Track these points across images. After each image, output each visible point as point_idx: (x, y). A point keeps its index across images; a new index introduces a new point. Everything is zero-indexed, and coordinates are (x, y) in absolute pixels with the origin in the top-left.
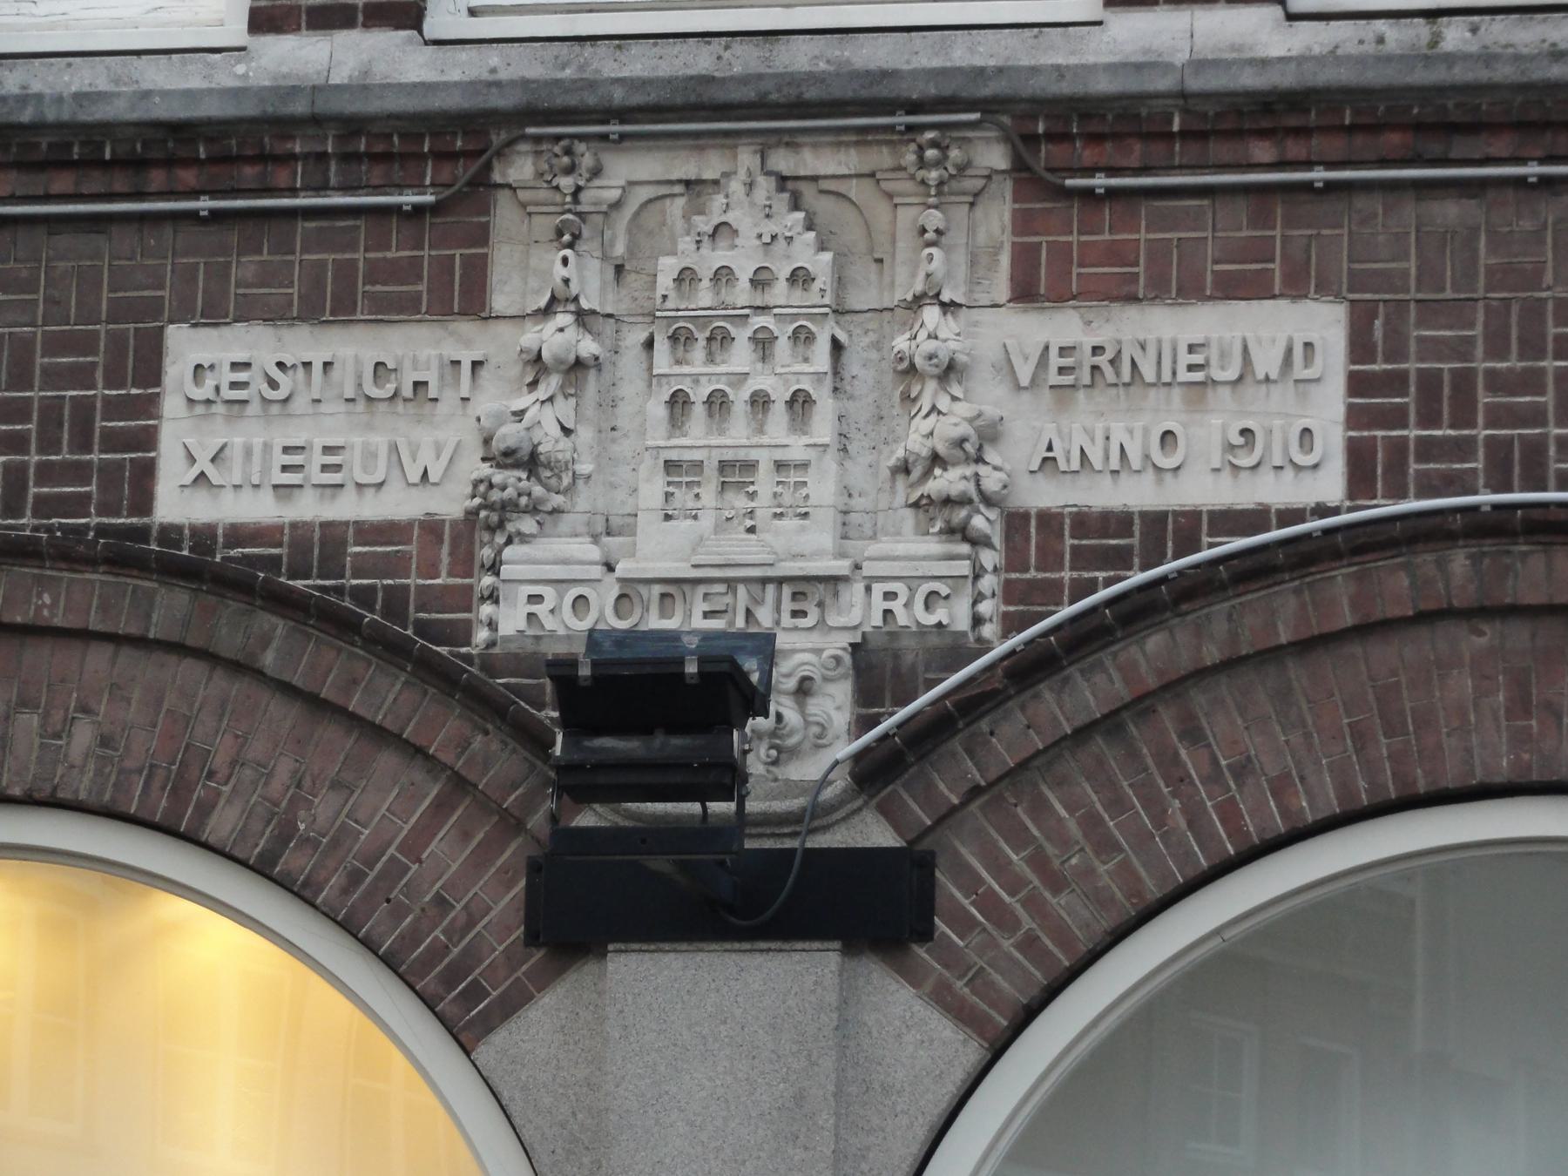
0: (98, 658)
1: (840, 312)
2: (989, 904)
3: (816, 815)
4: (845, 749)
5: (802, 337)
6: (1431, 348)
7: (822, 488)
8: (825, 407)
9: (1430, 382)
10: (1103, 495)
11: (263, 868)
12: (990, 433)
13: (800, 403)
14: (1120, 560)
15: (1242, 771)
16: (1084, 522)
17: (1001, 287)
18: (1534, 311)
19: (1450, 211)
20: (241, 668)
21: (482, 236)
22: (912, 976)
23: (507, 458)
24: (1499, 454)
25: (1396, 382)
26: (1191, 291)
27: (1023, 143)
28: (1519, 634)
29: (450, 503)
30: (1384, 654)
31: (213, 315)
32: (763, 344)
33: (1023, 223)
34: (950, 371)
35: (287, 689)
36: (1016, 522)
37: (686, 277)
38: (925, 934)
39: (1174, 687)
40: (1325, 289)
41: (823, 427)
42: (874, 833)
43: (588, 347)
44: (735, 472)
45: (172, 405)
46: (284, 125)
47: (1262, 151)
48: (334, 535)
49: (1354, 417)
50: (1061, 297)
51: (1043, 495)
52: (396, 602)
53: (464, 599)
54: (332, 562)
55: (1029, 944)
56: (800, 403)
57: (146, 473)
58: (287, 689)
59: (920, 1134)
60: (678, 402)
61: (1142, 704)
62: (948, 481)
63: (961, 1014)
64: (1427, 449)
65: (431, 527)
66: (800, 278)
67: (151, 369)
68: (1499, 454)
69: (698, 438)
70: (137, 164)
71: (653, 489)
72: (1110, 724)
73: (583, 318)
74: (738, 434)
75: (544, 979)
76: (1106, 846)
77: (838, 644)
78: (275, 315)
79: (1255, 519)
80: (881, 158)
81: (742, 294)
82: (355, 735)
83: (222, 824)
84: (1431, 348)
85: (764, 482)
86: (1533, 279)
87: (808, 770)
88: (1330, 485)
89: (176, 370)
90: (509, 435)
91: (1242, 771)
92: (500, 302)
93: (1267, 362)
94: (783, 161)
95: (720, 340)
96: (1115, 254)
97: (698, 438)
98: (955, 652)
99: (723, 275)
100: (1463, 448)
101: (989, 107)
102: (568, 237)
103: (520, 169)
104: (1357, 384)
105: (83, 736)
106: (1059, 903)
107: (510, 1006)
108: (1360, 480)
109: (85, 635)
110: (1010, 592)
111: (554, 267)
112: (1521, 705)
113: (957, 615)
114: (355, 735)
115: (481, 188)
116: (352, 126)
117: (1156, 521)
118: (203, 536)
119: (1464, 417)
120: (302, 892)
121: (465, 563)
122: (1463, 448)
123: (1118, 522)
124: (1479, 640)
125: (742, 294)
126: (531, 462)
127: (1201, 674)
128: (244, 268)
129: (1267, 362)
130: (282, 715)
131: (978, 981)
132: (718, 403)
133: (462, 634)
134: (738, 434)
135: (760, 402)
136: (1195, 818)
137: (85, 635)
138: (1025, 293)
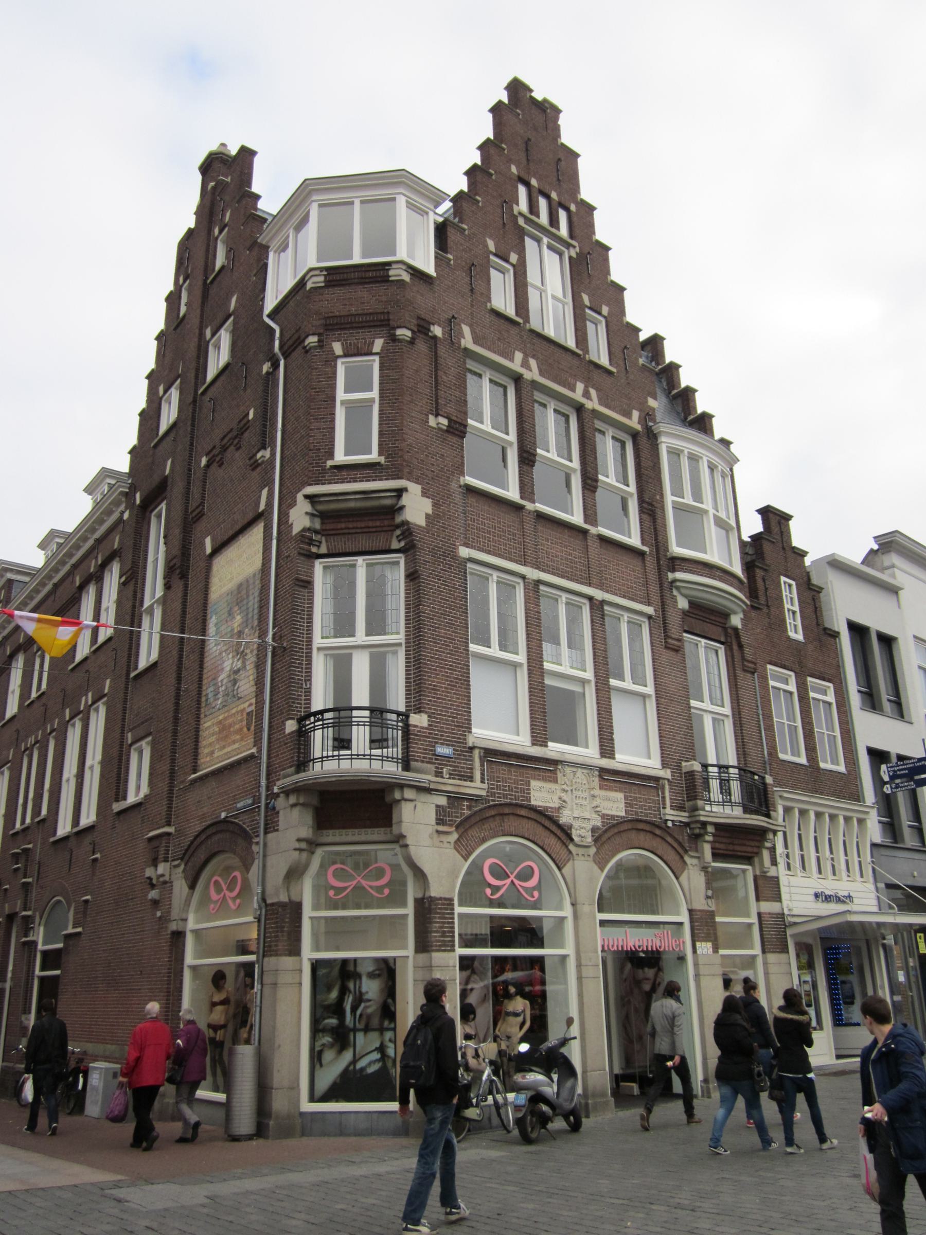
31: (535, 779)
65: (555, 808)
70: (527, 760)
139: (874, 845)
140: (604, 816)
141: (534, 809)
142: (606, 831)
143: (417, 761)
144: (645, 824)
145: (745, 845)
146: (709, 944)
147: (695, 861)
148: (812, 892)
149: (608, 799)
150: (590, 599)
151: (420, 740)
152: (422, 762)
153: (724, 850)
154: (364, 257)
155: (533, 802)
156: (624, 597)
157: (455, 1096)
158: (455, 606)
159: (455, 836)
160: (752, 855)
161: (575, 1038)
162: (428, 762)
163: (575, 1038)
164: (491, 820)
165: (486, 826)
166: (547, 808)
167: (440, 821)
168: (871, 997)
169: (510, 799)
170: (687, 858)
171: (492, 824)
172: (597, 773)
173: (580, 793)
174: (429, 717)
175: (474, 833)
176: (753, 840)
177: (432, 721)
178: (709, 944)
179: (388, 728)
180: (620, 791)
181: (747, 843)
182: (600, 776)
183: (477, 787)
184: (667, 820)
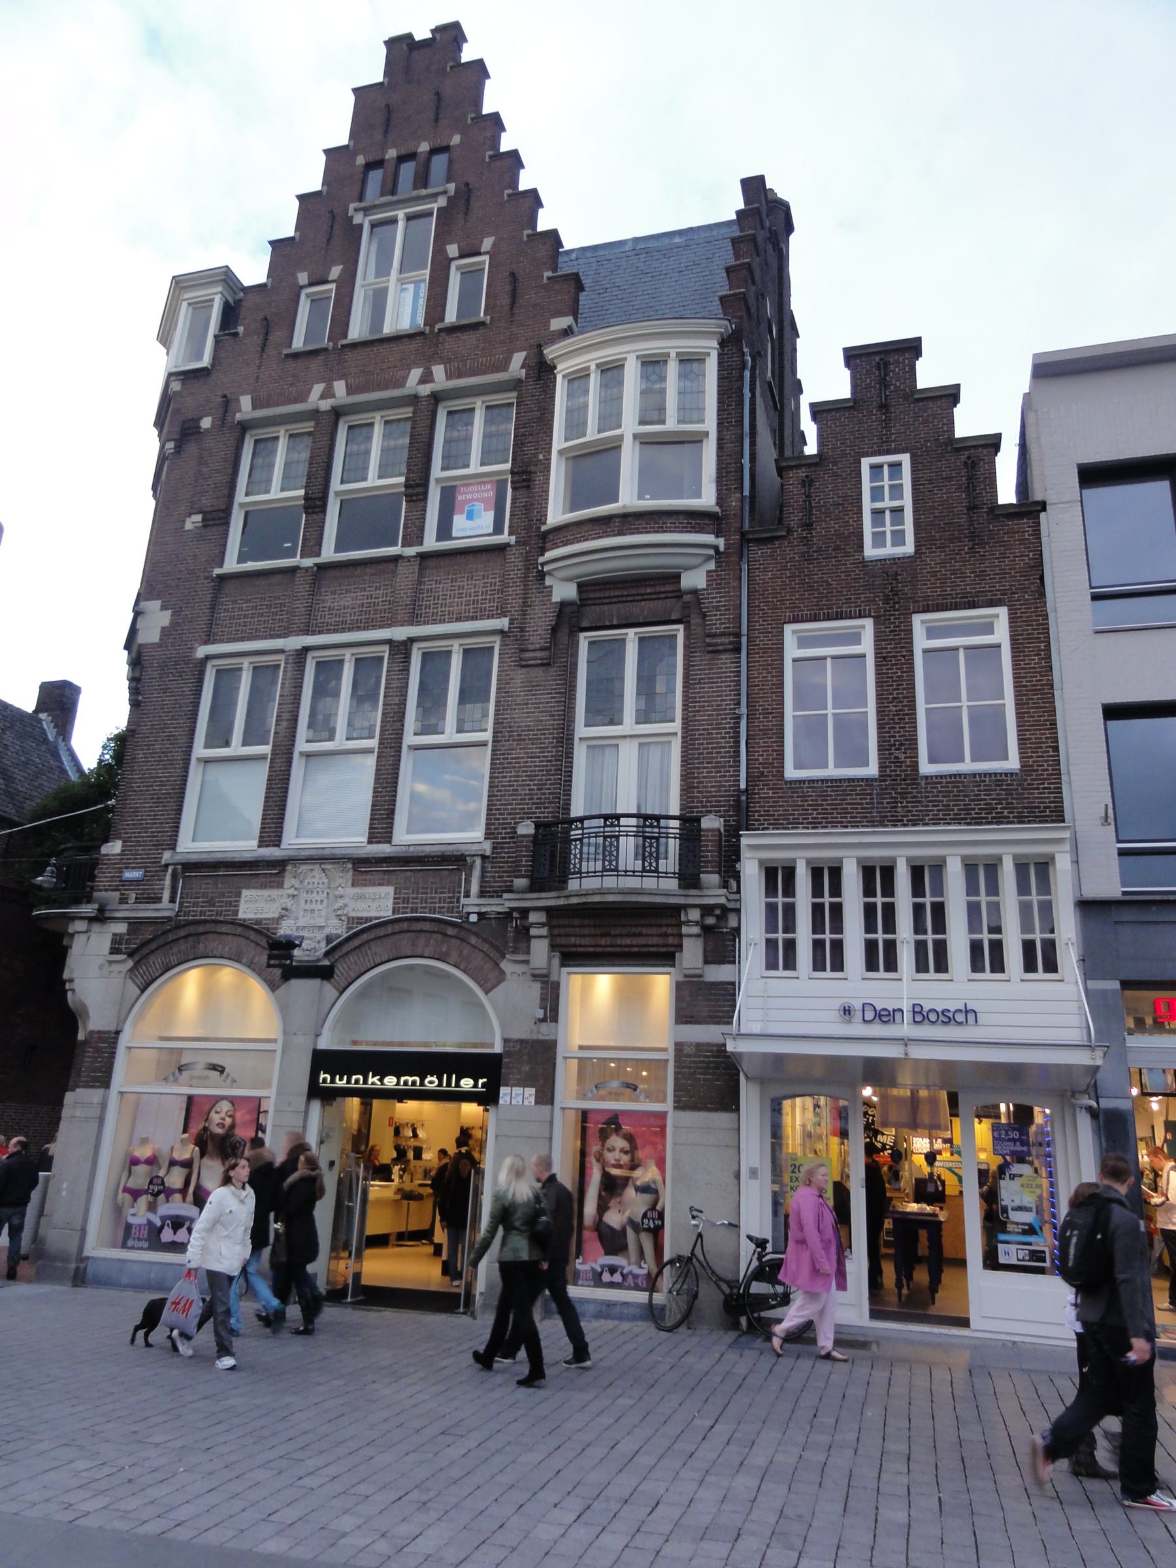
0: (230, 938)
1: (329, 888)
2: (341, 973)
3: (318, 960)
4: (324, 950)
5: (323, 892)
6: (405, 894)
7: (323, 913)
8: (325, 901)
9: (404, 898)
10: (360, 914)
11: (249, 967)
12: (346, 906)
13: (322, 901)
14: (361, 924)
15: (376, 953)
16: (358, 918)
17: (350, 884)
18: (418, 888)
19: (409, 874)
20: (248, 938)
21: (284, 877)
22: (331, 983)
23: (283, 909)
24: (412, 908)
25: (399, 898)
26: (374, 885)
27: (354, 864)
28: (413, 934)
29: (276, 915)
30: (397, 937)
31: (248, 888)
32: (318, 892)
33: (353, 875)
34: (341, 897)
35: (253, 941)
36: (349, 918)
37: (309, 883)
38: (332, 977)
39: (367, 942)
40: (392, 885)
41: (324, 904)
42: (326, 963)
43: (296, 893)
44: (313, 911)
45: (242, 901)
46: (260, 861)
47: (384, 865)
48: (261, 920)
49: (394, 903)
50: (357, 886)
51: (353, 914)
52: (268, 929)
53: (276, 929)
54: (260, 924)
55: (346, 979)
56: (322, 901)
57: (238, 911)
58: (253, 941)
59: (330, 1006)
60: (306, 901)
61: (191, 935)
62: (339, 912)
63: (336, 988)
64: (403, 908)
65: (274, 919)
66: (323, 883)
67: (239, 895)
68: (412, 908)
69: (308, 906)
70: (240, 867)
71: (302, 913)
72: (359, 947)
73: (296, 889)
74: (313, 906)
75: (283, 983)
76: (357, 964)
77: (324, 935)
78: (256, 888)
79: (380, 918)
80: (336, 866)
81: (316, 885)
82: (510, 1196)
83: (244, 960)
84: (405, 894)
85: (316, 912)
86: (418, 884)
87: (318, 954)
88: (390, 913)
89: (243, 896)
90: (284, 906)
91: (376, 953)
92: (285, 886)
93: (383, 896)
94: (323, 866)
95: (312, 892)
96: (365, 880)
97: (308, 906)
98: (339, 936)
99: (313, 883)
100: (407, 908)
101: (349, 859)
102: (295, 877)
103: (289, 868)
104: (395, 898)
105: (227, 949)
106: (350, 973)
107: (279, 987)
108: (394, 913)
109: (228, 934)
110: (348, 928)
111: (294, 881)
112: (413, 945)
113: (339, 932)
114: (510, 1196)
115: (284, 870)
116: (268, 862)
117: (367, 918)
118: (244, 920)
119: (440, 898)
120: (254, 970)
121: (278, 924)
122: (407, 908)
123: (362, 918)
124: (407, 935)
125: (316, 885)
126: (286, 909)
127: (371, 940)
128: (253, 881)
129: (383, 896)
130: (253, 945)
131: (339, 984)
132: (311, 901)
133: (275, 934)
134: (313, 906)
135: (317, 901)
136: (369, 961)
137: (228, 934)
138: (353, 885)
139: (1088, 907)
140: (351, 920)
141: (245, 926)
142: (348, 939)
143: (101, 890)
144: (679, 897)
145: (640, 935)
146: (531, 1092)
147: (520, 968)
148: (837, 1004)
149: (360, 897)
150: (389, 642)
151: (108, 868)
152: (106, 890)
153: (591, 946)
154: (574, 507)
155: (241, 915)
156: (458, 619)
157: (293, 1186)
158: (179, 715)
159: (130, 964)
160: (673, 949)
161: (966, 1004)
162: (112, 890)
163: (966, 1004)
164: (182, 941)
165: (175, 949)
166: (258, 922)
167: (114, 950)
168: (996, 1236)
169: (193, 916)
170: (504, 965)
171: (183, 946)
172: (350, 866)
173: (315, 894)
174: (124, 842)
175: (157, 960)
176: (651, 925)
177: (127, 846)
178: (531, 1092)
179: (667, 837)
180: (388, 883)
181: (645, 931)
182: (355, 869)
183: (165, 908)
184: (469, 913)
